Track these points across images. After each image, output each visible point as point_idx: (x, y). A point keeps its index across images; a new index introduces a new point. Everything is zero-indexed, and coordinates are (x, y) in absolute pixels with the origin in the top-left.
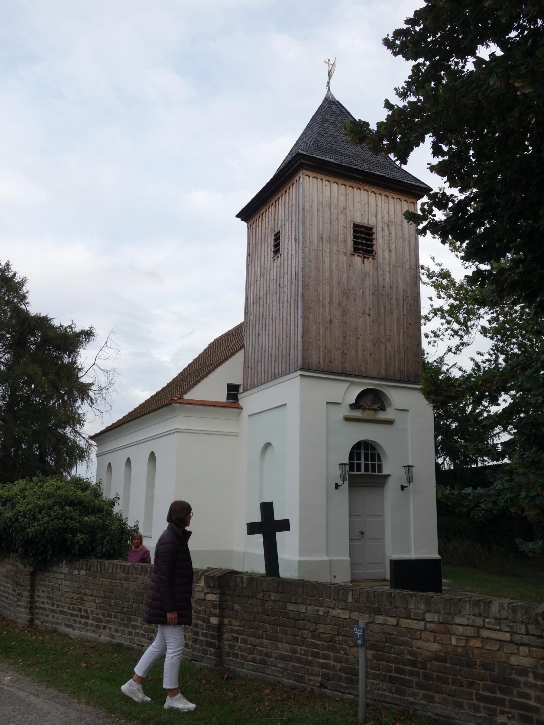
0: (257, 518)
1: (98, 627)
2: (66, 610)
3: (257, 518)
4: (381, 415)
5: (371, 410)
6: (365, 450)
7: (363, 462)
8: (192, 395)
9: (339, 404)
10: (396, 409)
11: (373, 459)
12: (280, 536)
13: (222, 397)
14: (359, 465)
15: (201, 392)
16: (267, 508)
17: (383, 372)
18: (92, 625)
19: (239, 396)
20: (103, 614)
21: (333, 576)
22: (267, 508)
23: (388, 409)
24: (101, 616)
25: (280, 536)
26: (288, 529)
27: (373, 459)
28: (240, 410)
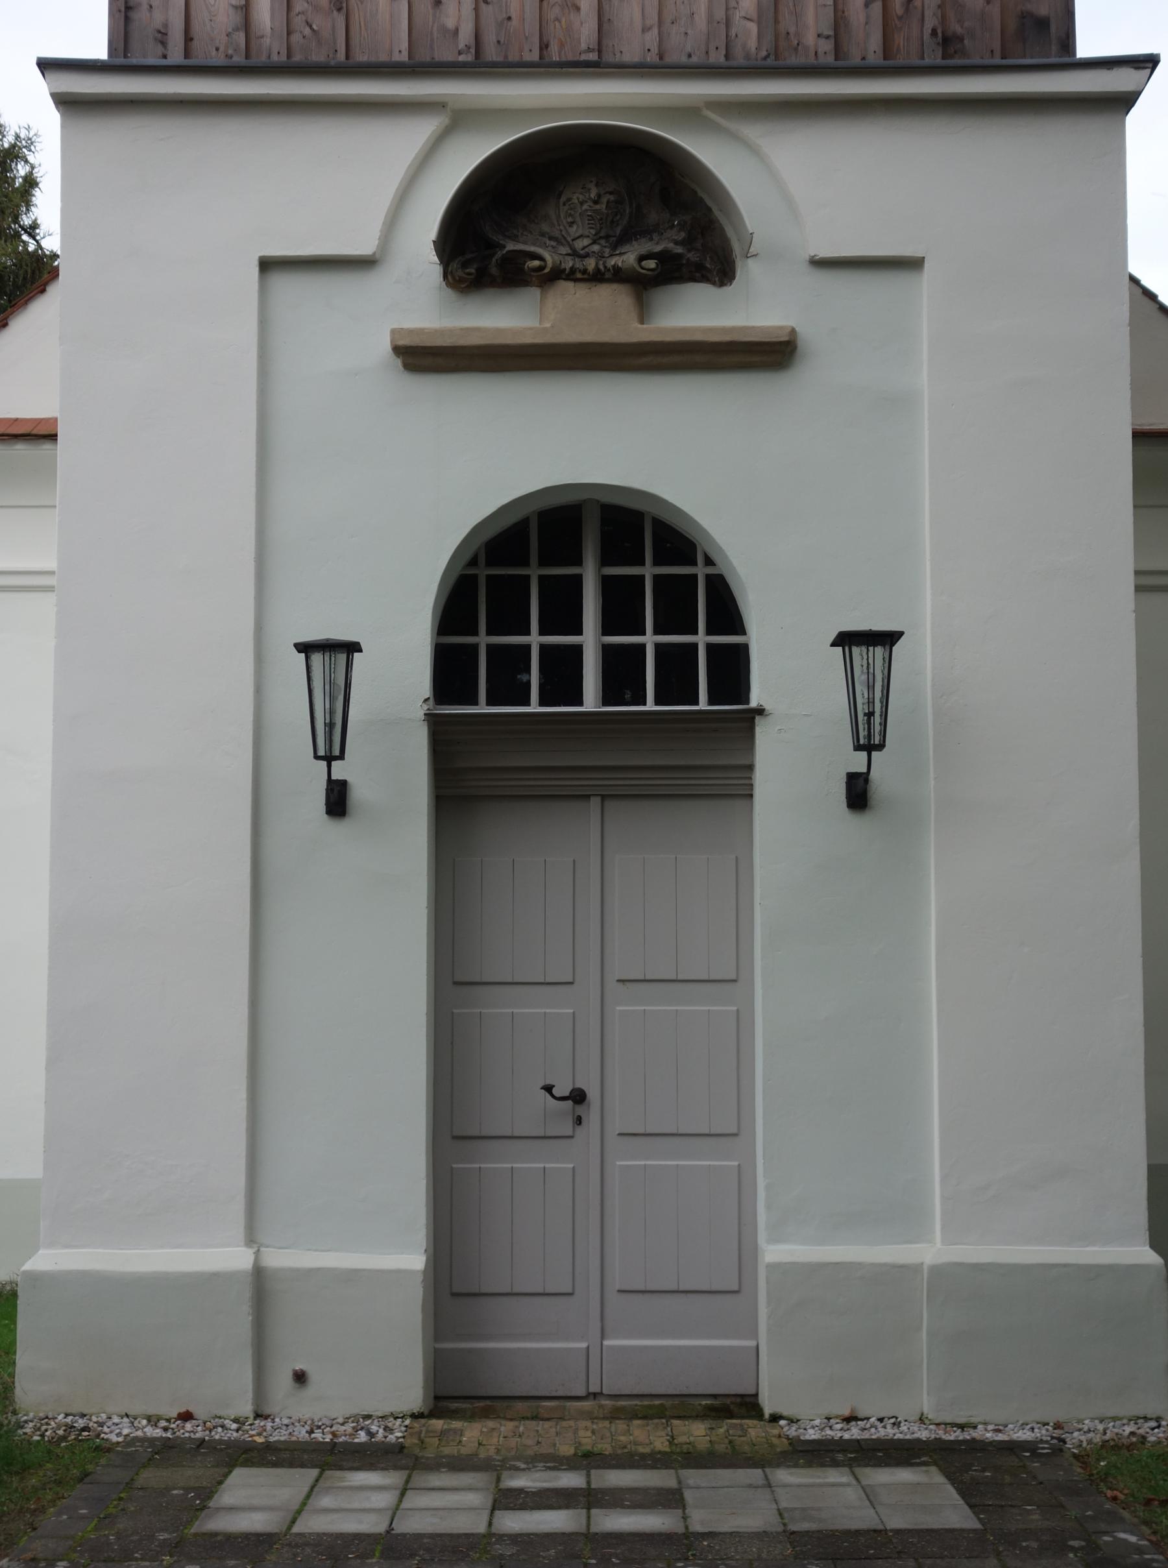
4: (693, 312)
5: (597, 277)
6: (606, 560)
7: (590, 640)
9: (364, 263)
10: (820, 263)
11: (676, 616)
17: (749, 36)
21: (287, 1379)
23: (749, 271)
27: (676, 616)
28: (47, 446)
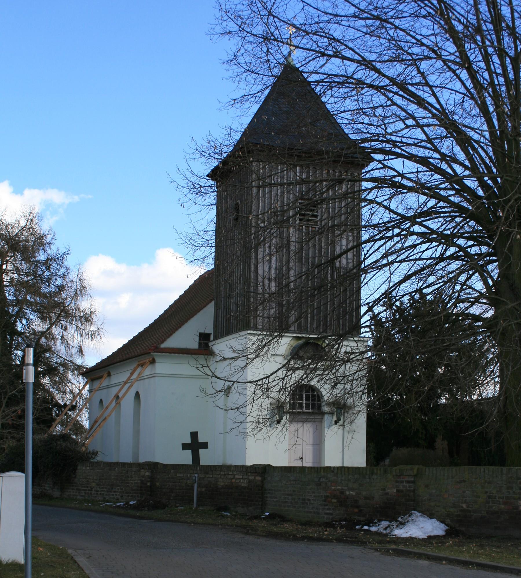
0: (188, 440)
1: (97, 494)
2: (80, 488)
3: (188, 440)
8: (172, 342)
12: (202, 452)
13: (194, 344)
14: (301, 406)
15: (175, 341)
16: (194, 435)
18: (94, 494)
19: (210, 344)
20: (100, 488)
22: (194, 435)
24: (98, 489)
25: (202, 452)
26: (207, 448)
